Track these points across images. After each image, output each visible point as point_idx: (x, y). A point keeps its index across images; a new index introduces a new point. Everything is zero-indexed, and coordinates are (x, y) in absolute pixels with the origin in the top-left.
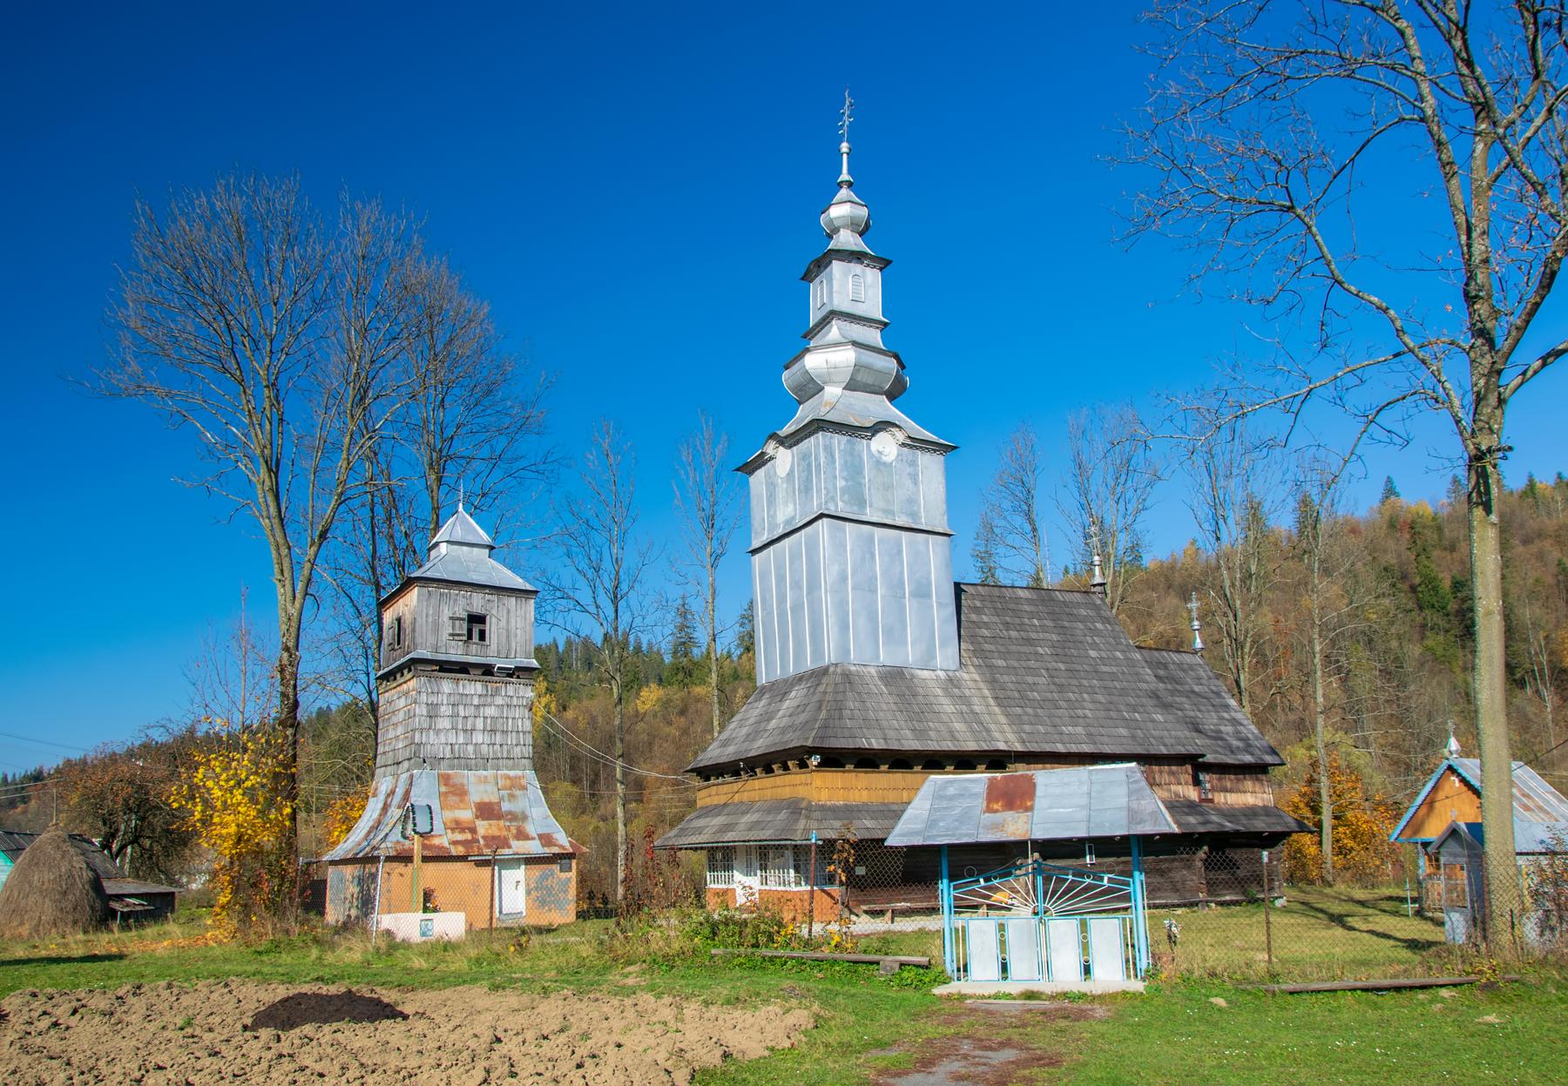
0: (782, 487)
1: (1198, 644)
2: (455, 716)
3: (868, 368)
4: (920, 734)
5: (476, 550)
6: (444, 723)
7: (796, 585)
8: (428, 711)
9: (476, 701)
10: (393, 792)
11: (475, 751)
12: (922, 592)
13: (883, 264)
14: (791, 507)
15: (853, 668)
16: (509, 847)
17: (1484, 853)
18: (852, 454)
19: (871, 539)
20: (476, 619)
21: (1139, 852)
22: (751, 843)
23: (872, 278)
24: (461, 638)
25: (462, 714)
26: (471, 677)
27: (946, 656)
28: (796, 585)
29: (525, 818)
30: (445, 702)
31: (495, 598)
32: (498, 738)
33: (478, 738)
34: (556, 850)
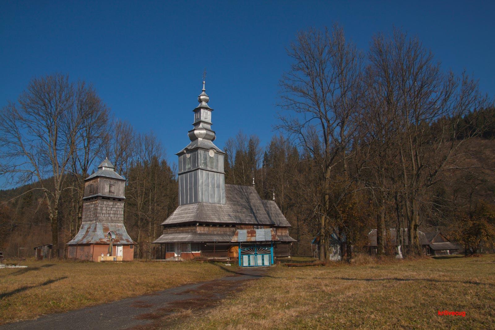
0: (187, 161)
1: (274, 199)
2: (107, 210)
3: (209, 135)
4: (219, 219)
5: (111, 169)
6: (104, 212)
7: (191, 183)
9: (111, 207)
10: (89, 228)
12: (218, 187)
13: (211, 110)
14: (190, 165)
15: (205, 204)
16: (120, 242)
17: (236, 155)
18: (205, 155)
19: (208, 174)
22: (301, 259)
23: (209, 113)
25: (108, 209)
27: (223, 201)
28: (191, 183)
29: (122, 235)
31: (116, 181)
32: (116, 216)
33: (112, 215)
34: (130, 243)
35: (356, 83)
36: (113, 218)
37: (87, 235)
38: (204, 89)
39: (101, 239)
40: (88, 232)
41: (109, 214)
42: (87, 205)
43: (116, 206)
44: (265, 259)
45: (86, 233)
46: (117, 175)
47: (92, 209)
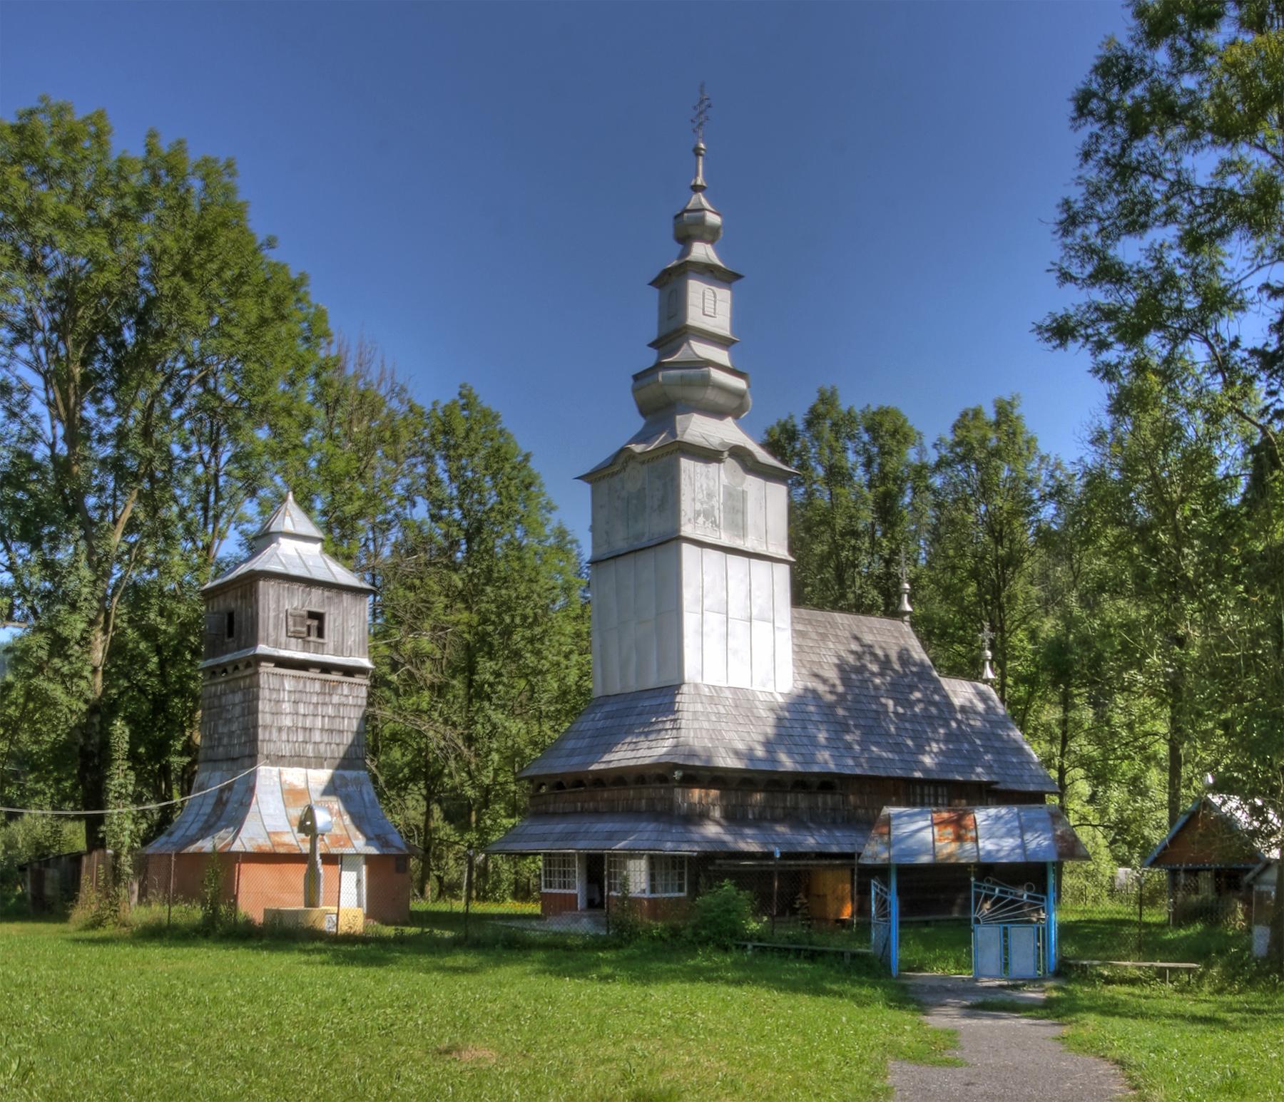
9: (315, 699)
20: (318, 617)
35: (1212, 998)
36: (322, 747)
37: (219, 818)
38: (700, 181)
39: (276, 833)
40: (225, 804)
41: (305, 729)
42: (215, 695)
43: (336, 699)
44: (1013, 943)
45: (214, 810)
46: (342, 575)
47: (238, 711)
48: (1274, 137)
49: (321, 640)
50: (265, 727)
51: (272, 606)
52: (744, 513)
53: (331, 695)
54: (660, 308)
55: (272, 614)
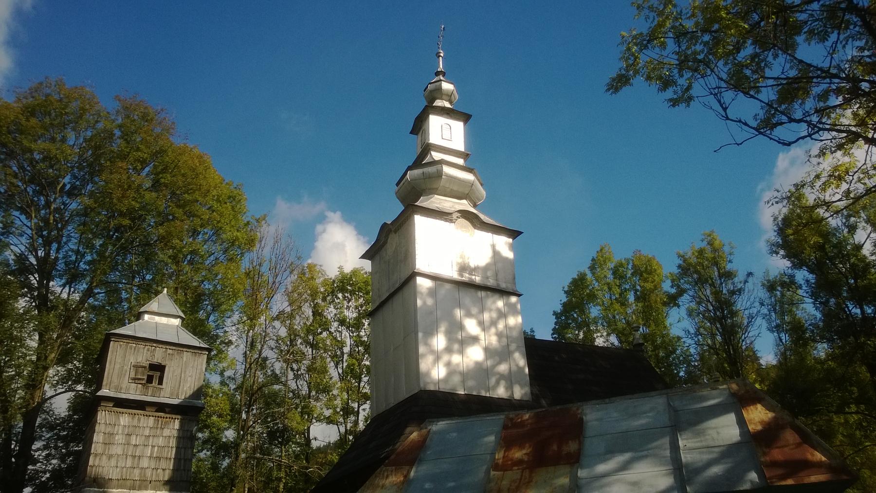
6: (117, 450)
8: (104, 439)
9: (147, 432)
11: (140, 474)
13: (465, 117)
20: (159, 368)
21: (12, 199)
23: (458, 127)
24: (141, 382)
26: (148, 413)
30: (120, 432)
36: (149, 473)
41: (134, 457)
48: (289, 399)
49: (160, 386)
50: (96, 455)
51: (119, 360)
52: (810, 65)
53: (162, 429)
54: (440, 146)
55: (117, 366)
